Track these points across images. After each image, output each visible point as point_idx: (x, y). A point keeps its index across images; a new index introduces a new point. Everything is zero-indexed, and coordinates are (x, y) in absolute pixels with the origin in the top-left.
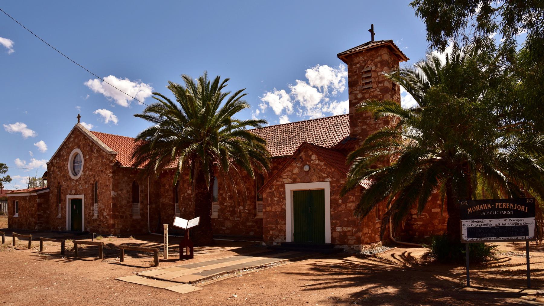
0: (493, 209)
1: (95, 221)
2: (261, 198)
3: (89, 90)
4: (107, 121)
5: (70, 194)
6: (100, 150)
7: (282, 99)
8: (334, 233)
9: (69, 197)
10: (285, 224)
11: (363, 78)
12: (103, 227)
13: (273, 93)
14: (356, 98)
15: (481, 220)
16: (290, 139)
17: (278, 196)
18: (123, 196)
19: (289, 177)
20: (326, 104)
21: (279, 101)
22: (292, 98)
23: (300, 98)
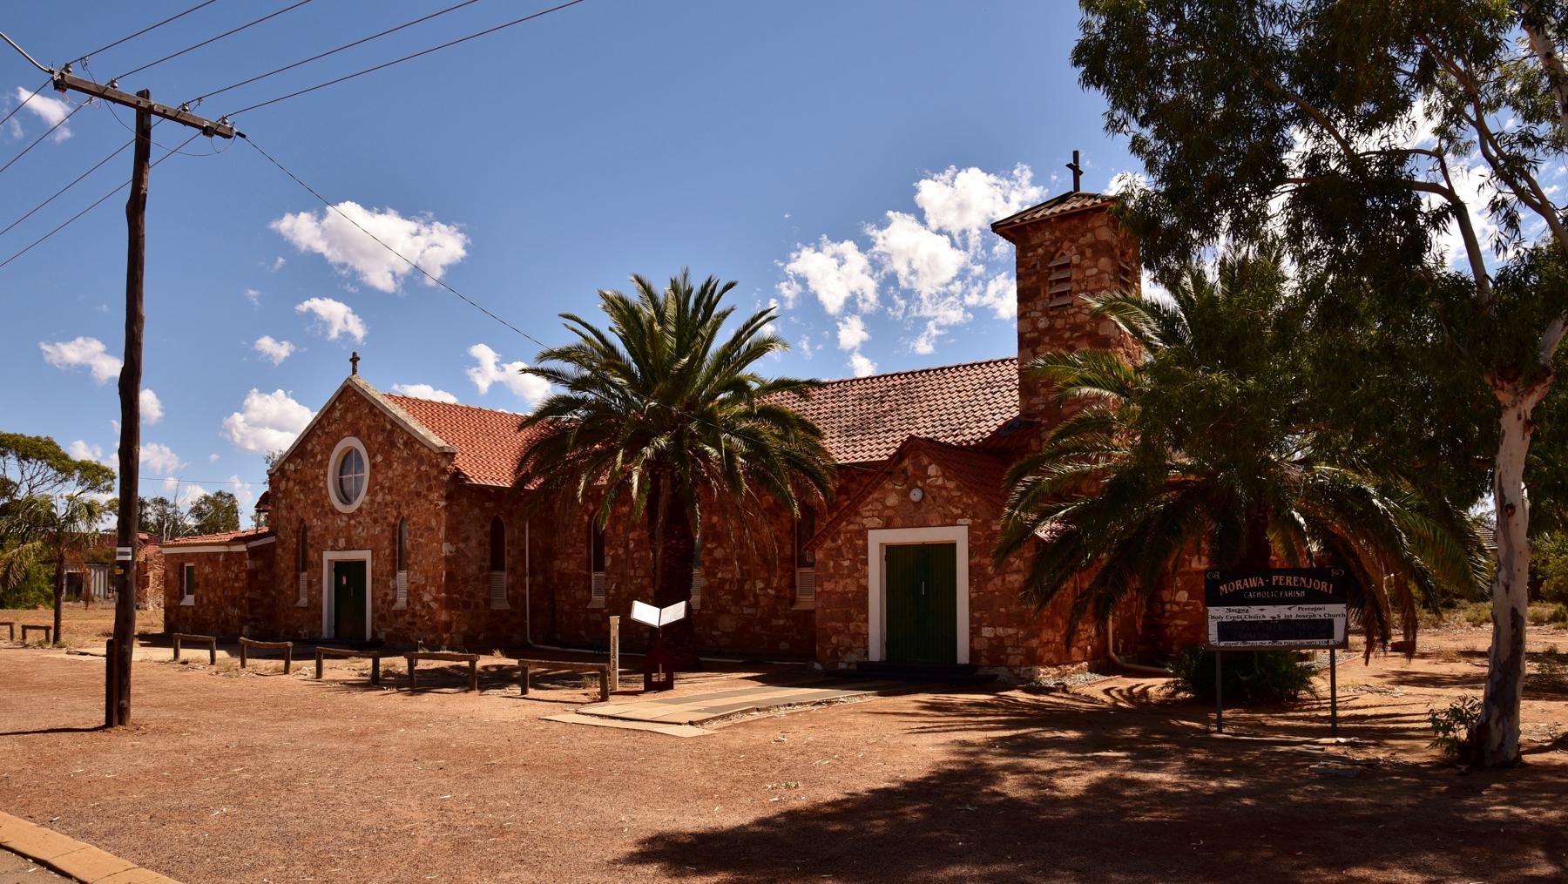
0: (1268, 587)
1: (401, 615)
2: (811, 561)
3: (285, 245)
4: (334, 334)
5: (333, 549)
6: (412, 440)
7: (845, 268)
8: (976, 640)
9: (329, 556)
10: (866, 620)
11: (1051, 282)
12: (420, 630)
13: (818, 250)
14: (1035, 329)
15: (1245, 608)
16: (877, 418)
17: (850, 557)
18: (470, 555)
19: (876, 513)
20: (975, 284)
21: (837, 274)
22: (876, 265)
23: (901, 267)
